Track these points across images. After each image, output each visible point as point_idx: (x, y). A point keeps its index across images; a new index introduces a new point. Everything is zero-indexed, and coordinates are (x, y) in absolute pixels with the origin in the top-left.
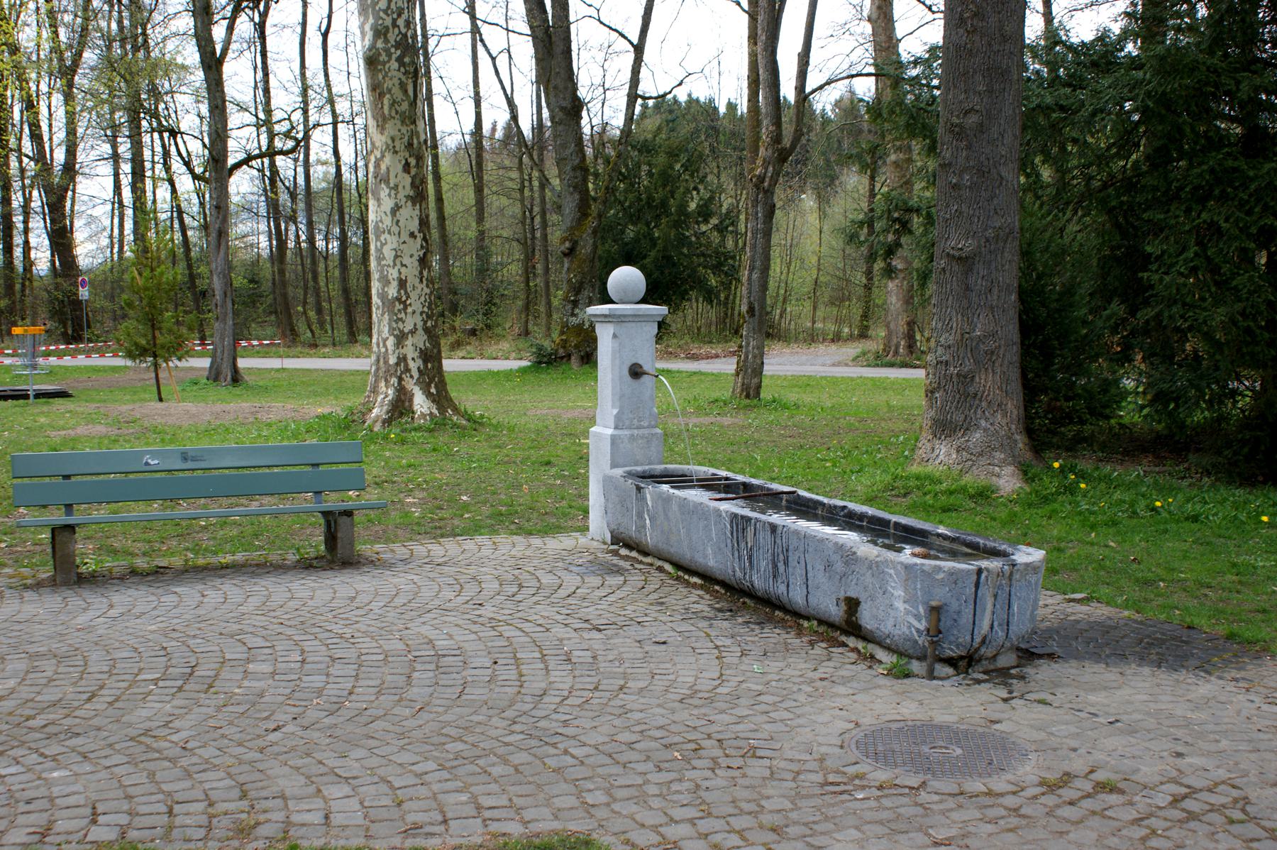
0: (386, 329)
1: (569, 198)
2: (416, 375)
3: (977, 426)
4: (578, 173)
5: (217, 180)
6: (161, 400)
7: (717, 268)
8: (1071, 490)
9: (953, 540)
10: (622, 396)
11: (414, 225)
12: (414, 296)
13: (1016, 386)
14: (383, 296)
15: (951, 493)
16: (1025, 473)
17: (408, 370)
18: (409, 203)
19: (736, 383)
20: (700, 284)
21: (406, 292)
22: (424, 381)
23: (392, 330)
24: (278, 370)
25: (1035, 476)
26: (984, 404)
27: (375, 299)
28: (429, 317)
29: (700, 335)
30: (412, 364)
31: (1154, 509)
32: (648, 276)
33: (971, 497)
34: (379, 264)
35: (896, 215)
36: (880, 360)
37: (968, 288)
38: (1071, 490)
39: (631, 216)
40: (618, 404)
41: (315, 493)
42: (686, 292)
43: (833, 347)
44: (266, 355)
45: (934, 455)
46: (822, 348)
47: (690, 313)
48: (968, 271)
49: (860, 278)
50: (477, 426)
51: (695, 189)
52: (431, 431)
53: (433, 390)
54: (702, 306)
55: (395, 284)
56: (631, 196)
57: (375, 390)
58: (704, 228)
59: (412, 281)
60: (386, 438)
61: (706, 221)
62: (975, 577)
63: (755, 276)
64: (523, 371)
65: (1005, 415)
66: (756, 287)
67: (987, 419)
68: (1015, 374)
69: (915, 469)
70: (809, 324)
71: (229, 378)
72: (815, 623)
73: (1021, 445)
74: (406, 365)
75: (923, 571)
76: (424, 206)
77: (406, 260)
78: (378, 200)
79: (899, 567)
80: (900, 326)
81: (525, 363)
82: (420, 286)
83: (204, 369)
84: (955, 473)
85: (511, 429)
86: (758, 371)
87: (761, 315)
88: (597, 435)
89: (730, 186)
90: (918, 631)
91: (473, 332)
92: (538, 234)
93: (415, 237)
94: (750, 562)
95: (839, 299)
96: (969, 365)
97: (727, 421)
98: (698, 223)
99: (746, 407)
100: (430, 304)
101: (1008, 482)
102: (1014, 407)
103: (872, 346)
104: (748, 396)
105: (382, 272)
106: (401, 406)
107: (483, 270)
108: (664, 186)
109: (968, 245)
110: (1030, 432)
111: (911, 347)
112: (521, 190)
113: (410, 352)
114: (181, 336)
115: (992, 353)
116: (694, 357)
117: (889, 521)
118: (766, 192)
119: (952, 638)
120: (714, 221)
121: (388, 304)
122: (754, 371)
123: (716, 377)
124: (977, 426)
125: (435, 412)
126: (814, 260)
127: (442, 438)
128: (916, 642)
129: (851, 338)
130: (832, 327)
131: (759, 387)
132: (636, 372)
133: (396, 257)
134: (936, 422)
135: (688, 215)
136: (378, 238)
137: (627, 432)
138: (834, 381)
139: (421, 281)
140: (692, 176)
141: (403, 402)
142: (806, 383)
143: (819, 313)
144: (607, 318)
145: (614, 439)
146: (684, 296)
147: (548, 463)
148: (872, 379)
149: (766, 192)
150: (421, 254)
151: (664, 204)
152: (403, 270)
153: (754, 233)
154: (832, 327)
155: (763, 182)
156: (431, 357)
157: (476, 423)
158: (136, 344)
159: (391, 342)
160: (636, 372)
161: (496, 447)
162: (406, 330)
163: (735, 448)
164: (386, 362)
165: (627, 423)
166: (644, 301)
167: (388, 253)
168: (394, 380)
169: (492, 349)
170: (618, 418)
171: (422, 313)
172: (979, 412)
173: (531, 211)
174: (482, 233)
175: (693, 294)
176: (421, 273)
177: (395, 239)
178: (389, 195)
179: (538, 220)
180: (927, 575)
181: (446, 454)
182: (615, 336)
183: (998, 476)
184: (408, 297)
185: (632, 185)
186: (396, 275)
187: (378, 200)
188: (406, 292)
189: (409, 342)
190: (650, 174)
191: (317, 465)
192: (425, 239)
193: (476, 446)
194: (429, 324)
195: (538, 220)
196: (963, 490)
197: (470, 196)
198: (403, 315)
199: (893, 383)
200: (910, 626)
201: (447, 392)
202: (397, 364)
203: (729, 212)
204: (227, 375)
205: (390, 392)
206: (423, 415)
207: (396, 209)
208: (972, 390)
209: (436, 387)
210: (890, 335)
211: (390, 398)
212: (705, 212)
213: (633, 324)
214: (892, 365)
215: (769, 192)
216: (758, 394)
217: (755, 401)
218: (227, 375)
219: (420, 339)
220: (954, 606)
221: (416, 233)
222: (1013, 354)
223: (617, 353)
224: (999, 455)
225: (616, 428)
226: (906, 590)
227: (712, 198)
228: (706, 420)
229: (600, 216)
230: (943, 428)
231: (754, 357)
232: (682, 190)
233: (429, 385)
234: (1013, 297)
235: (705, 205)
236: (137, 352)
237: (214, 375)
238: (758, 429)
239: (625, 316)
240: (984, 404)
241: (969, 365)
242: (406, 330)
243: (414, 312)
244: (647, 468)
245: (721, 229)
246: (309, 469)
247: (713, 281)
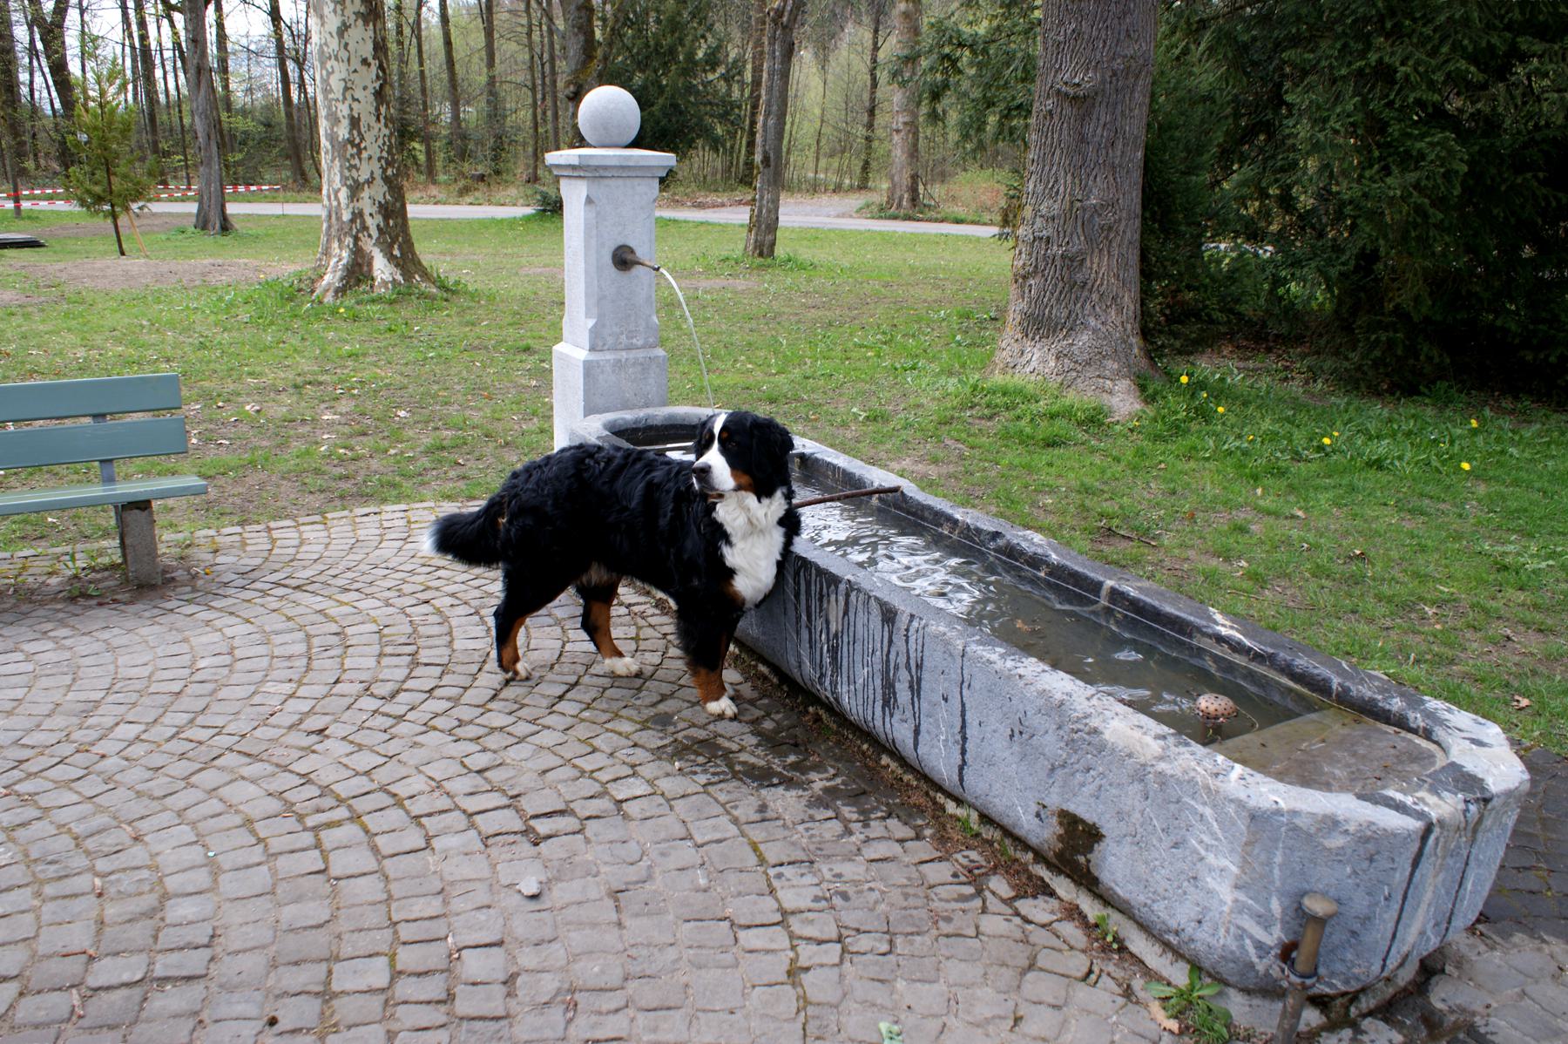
0: (338, 178)
1: (573, 40)
2: (375, 234)
3: (1085, 326)
4: (583, 13)
5: (191, 10)
6: (123, 253)
7: (724, 117)
8: (1204, 415)
9: (1258, 657)
10: (601, 299)
11: (367, 50)
12: (369, 137)
13: (1133, 274)
14: (332, 138)
15: (1053, 416)
16: (1143, 388)
17: (365, 228)
18: (360, 22)
19: (748, 240)
20: (707, 132)
21: (360, 133)
22: (385, 241)
23: (344, 179)
24: (278, 217)
25: (1156, 393)
26: (1095, 296)
27: (324, 143)
28: (389, 164)
29: (706, 184)
30: (369, 221)
31: (1321, 448)
32: (643, 101)
33: (1080, 424)
34: (326, 98)
35: (947, 50)
36: (883, 212)
37: (1083, 139)
38: (1204, 415)
39: (639, 63)
40: (595, 311)
41: (101, 461)
42: (693, 140)
43: (836, 198)
44: (273, 200)
45: (1023, 360)
46: (825, 198)
47: (696, 162)
48: (1083, 118)
49: (861, 131)
50: (449, 295)
51: (703, 37)
52: (392, 302)
53: (396, 252)
54: (709, 155)
55: (345, 123)
56: (638, 42)
57: (327, 252)
58: (711, 77)
59: (367, 119)
60: (334, 312)
61: (713, 70)
62: (1417, 845)
63: (771, 122)
64: (528, 219)
65: (1120, 311)
66: (771, 134)
67: (1097, 317)
68: (1134, 257)
69: (998, 379)
70: (811, 175)
71: (218, 226)
72: (974, 816)
73: (1136, 351)
74: (363, 222)
75: (1295, 829)
76: (379, 25)
77: (359, 94)
78: (322, 17)
79: (1231, 809)
80: (904, 180)
81: (530, 211)
82: (376, 126)
83: (189, 214)
84: (1053, 384)
85: (491, 298)
86: (772, 226)
87: (776, 166)
88: (565, 358)
89: (736, 34)
90: (1259, 946)
91: (482, 178)
92: (547, 80)
93: (369, 65)
94: (834, 659)
95: (842, 149)
96: (1079, 243)
97: (740, 284)
98: (705, 71)
99: (760, 267)
100: (390, 147)
101: (1123, 402)
102: (1130, 300)
103: (878, 198)
104: (761, 255)
105: (329, 108)
106: (358, 272)
107: (495, 113)
108: (673, 32)
109: (1087, 80)
110: (1145, 333)
111: (914, 200)
112: (529, 34)
113: (368, 207)
114: (139, 183)
115: (1110, 228)
116: (701, 206)
117: (1096, 587)
118: (784, 28)
119: (1339, 967)
120: (721, 70)
121: (339, 147)
122: (768, 226)
123: (724, 227)
124: (1085, 326)
125: (400, 278)
126: (817, 111)
127: (406, 312)
128: (1252, 966)
129: (851, 188)
130: (834, 178)
131: (773, 244)
132: (624, 259)
133: (346, 89)
134: (1027, 316)
135: (696, 63)
136: (323, 64)
137: (609, 356)
138: (843, 234)
139: (378, 119)
140: (700, 23)
141: (360, 265)
142: (815, 236)
143: (823, 163)
144: (579, 171)
145: (589, 369)
146: (690, 144)
147: (527, 349)
148: (880, 233)
149: (784, 28)
150: (377, 85)
151: (672, 51)
152: (355, 105)
153: (771, 74)
154: (834, 178)
155: (781, 16)
156: (393, 212)
157: (449, 291)
158: (88, 192)
159: (344, 194)
160: (624, 259)
161: (467, 324)
162: (361, 180)
163: (753, 324)
164: (339, 218)
165: (610, 341)
166: (636, 143)
167: (336, 85)
168: (349, 240)
169: (500, 195)
170: (595, 333)
171: (380, 159)
172: (1088, 306)
173: (541, 58)
174: (492, 81)
175: (700, 142)
176: (377, 109)
177: (344, 66)
178: (335, 11)
179: (547, 66)
180: (1305, 836)
181: (403, 337)
182: (589, 201)
183: (1111, 393)
184: (362, 139)
185: (640, 31)
186: (346, 112)
187: (322, 17)
188: (360, 133)
189: (365, 194)
190: (658, 21)
191: (103, 416)
192: (381, 67)
193: (446, 323)
194: (389, 172)
195: (547, 66)
196: (1067, 413)
197: (479, 40)
198: (357, 161)
199: (901, 237)
200: (1242, 933)
201: (414, 254)
202: (352, 221)
203: (735, 61)
204: (213, 222)
205: (345, 254)
206: (384, 283)
207: (343, 29)
208: (1079, 277)
209: (400, 248)
210: (892, 191)
211: (344, 261)
212: (712, 61)
213: (620, 182)
214: (895, 218)
215: (787, 29)
216: (772, 252)
217: (769, 260)
218: (213, 222)
219: (379, 191)
220: (1360, 903)
221: (370, 59)
222: (1130, 231)
223: (593, 229)
224: (1112, 365)
225: (592, 349)
226: (1245, 864)
227: (719, 47)
228: (718, 283)
229: (606, 58)
230: (1038, 325)
231: (769, 211)
232: (690, 37)
233: (391, 246)
234: (1140, 154)
235: (713, 54)
236: (93, 201)
237: (203, 223)
238: (776, 296)
239: (606, 168)
240: (1095, 296)
241: (1079, 243)
242: (361, 180)
243: (370, 158)
244: (641, 413)
245: (727, 78)
246: (88, 421)
247: (719, 130)
